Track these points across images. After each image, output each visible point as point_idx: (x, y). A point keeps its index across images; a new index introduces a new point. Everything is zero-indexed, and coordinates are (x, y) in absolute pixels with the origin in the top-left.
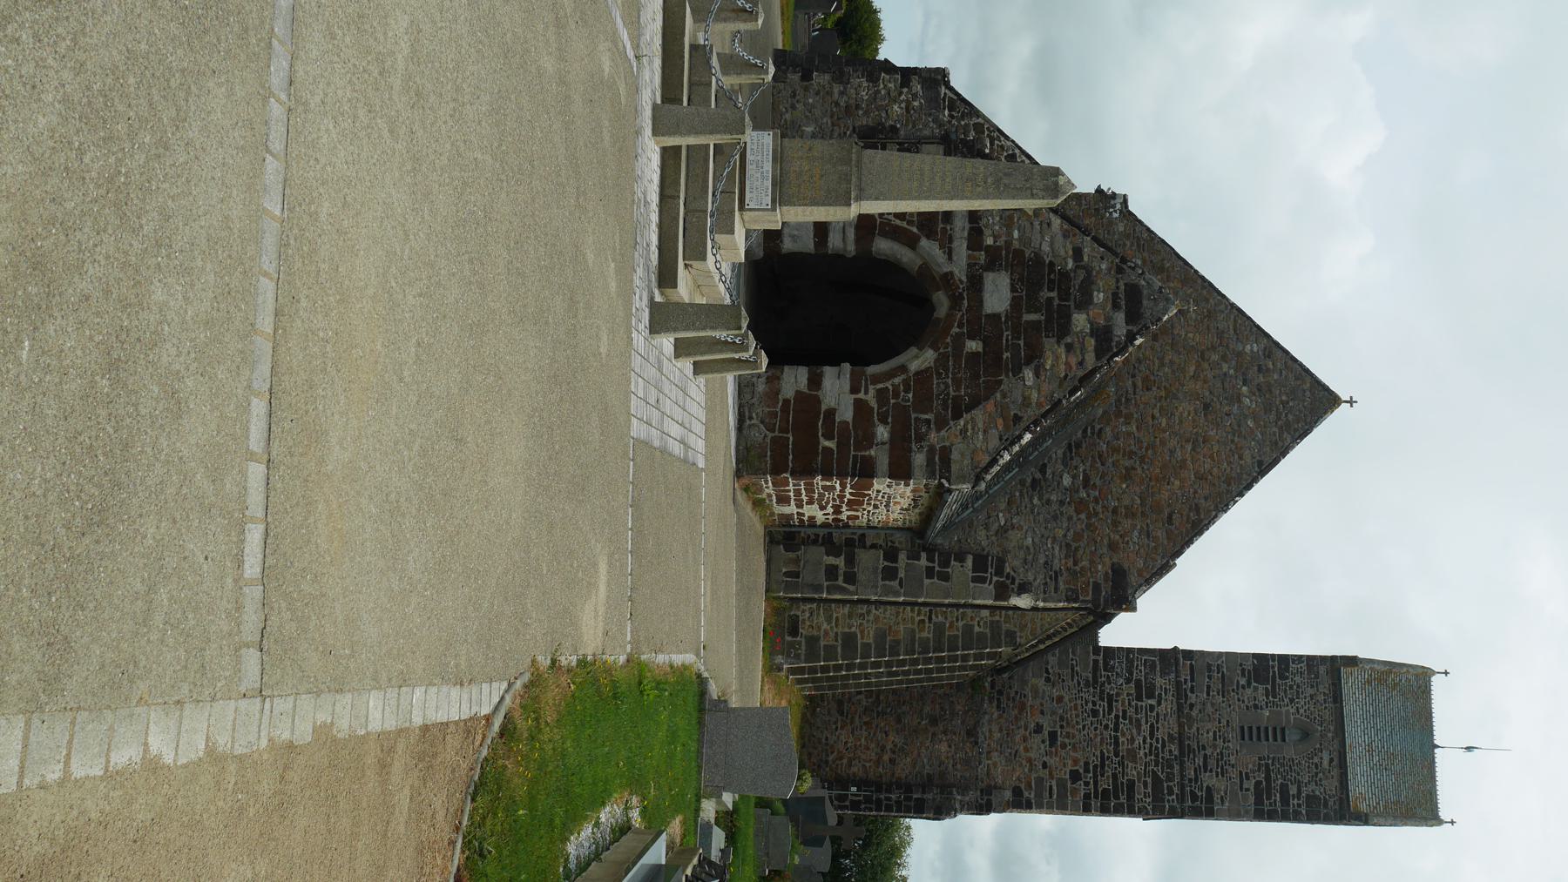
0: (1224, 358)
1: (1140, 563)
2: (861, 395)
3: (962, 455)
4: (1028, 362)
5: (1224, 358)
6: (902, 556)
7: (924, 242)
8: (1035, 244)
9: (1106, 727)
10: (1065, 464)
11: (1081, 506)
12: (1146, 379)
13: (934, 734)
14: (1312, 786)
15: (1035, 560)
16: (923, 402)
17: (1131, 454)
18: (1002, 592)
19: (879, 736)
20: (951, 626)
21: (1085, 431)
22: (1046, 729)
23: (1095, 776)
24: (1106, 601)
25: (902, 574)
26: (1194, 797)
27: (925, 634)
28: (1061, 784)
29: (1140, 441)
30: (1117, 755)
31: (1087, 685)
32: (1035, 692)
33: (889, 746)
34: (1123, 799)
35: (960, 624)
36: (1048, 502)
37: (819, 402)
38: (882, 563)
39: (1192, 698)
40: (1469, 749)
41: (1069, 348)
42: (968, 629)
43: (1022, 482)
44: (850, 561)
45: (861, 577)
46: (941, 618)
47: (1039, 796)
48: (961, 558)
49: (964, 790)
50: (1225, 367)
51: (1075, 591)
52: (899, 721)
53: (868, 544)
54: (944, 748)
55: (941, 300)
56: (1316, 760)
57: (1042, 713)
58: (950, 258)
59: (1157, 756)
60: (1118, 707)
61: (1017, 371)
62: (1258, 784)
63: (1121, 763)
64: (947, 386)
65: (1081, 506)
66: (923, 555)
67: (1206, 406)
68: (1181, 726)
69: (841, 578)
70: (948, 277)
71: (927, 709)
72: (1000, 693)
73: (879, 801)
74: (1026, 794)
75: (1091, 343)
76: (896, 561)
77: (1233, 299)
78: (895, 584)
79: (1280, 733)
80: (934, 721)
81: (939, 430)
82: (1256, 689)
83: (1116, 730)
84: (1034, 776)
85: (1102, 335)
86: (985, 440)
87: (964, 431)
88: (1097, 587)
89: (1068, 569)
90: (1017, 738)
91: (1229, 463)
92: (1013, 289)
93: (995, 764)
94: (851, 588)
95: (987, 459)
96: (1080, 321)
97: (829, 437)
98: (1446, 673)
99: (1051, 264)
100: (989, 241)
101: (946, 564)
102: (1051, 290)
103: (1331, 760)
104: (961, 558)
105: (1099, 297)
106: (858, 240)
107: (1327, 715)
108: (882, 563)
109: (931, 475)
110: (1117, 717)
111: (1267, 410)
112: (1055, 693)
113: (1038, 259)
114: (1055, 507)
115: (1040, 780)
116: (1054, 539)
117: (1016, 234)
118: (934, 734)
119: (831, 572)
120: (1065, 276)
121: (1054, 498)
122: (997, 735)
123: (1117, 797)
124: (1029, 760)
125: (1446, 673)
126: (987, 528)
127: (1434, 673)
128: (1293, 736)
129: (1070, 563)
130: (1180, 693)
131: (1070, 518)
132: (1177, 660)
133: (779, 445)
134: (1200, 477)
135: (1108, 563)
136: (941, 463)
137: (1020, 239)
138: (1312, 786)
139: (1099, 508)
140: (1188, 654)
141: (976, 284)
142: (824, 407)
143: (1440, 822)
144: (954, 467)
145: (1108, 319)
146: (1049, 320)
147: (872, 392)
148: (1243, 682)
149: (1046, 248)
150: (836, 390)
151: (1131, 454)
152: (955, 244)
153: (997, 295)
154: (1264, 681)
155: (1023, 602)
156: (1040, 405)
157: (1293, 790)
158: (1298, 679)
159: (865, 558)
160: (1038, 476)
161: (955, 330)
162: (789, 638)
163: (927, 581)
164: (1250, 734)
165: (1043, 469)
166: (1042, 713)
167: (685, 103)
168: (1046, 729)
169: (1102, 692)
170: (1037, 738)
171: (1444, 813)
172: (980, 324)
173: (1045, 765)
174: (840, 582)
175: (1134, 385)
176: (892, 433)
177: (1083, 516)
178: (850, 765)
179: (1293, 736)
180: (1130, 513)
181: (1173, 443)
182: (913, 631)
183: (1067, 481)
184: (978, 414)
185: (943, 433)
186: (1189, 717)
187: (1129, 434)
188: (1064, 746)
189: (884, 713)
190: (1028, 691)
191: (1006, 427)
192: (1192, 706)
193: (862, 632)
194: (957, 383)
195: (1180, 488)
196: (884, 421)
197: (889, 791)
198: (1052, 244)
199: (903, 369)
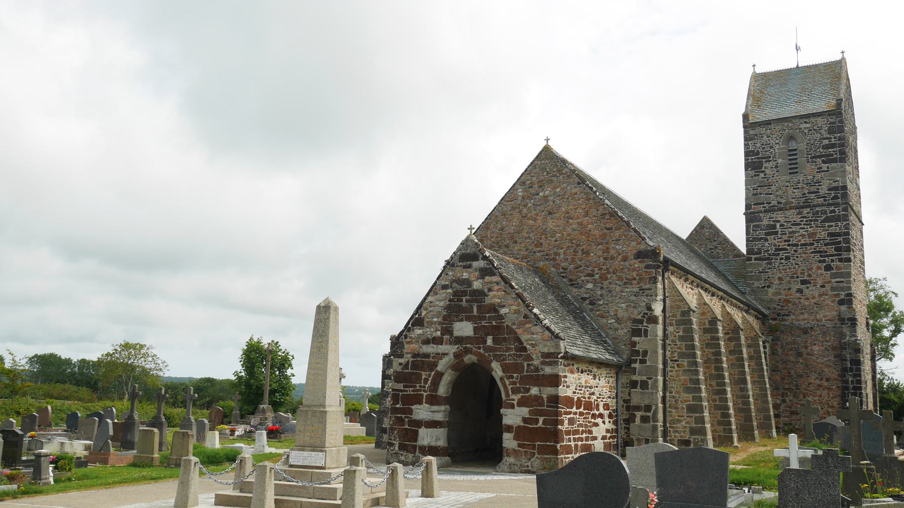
0: (525, 206)
1: (634, 244)
2: (515, 403)
3: (545, 346)
4: (497, 311)
5: (525, 206)
6: (634, 378)
7: (439, 368)
8: (440, 309)
9: (796, 251)
10: (581, 287)
11: (603, 278)
12: (536, 246)
13: (808, 354)
14: (823, 131)
15: (633, 302)
16: (517, 368)
17: (575, 252)
18: (653, 320)
19: (811, 388)
20: (679, 348)
21: (563, 277)
22: (800, 286)
23: (827, 256)
24: (655, 261)
25: (644, 378)
26: (836, 197)
27: (686, 364)
28: (834, 276)
29: (568, 247)
30: (813, 244)
31: (770, 264)
32: (777, 294)
33: (818, 382)
34: (840, 239)
35: (678, 343)
36: (601, 295)
37: (519, 426)
38: (638, 389)
39: (774, 203)
40: (797, 49)
41: (490, 290)
42: (681, 338)
43: (591, 310)
44: (638, 408)
45: (647, 402)
46: (676, 355)
47: (842, 289)
48: (634, 344)
49: (843, 335)
50: (530, 205)
51: (650, 279)
52: (801, 376)
53: (628, 398)
54: (816, 348)
55: (469, 359)
56: (806, 131)
57: (789, 289)
58: (447, 354)
59: (811, 221)
60: (782, 245)
61: (501, 317)
62: (824, 162)
63: (818, 241)
64: (510, 355)
65: (603, 278)
66: (633, 365)
67: (550, 213)
68: (791, 208)
69: (648, 414)
70: (456, 355)
71: (792, 359)
72: (779, 315)
73: (854, 388)
74: (842, 297)
75: (487, 279)
76: (637, 381)
77: (496, 203)
78: (650, 382)
79: (792, 152)
80: (799, 354)
81: (532, 359)
82: (766, 168)
83: (797, 245)
84: (830, 293)
85: (485, 273)
86: (537, 333)
87: (533, 345)
88: (647, 267)
89: (638, 283)
90: (807, 303)
91: (579, 199)
92: (462, 320)
93: (825, 316)
94: (653, 408)
95: (547, 332)
96: (477, 285)
97: (537, 421)
98: (754, 66)
99: (450, 301)
100: (439, 333)
101: (637, 353)
102: (462, 301)
103: (806, 122)
104: (634, 344)
105: (465, 275)
106: (439, 404)
107: (778, 128)
108: (638, 389)
109: (556, 363)
110: (789, 245)
111: (552, 182)
112: (777, 282)
113: (447, 308)
114: (604, 292)
115: (833, 289)
116: (622, 291)
117: (435, 320)
118: (808, 354)
119: (645, 419)
120: (455, 293)
121: (599, 293)
122: (806, 316)
123: (840, 243)
124: (820, 296)
125: (754, 66)
126: (616, 329)
127: (754, 72)
128: (793, 145)
129: (635, 282)
130: (771, 210)
131: (610, 283)
132: (752, 213)
133: (543, 450)
134: (587, 214)
135: (635, 261)
136: (550, 358)
137: (438, 317)
138: (823, 131)
139: (604, 267)
140: (748, 207)
141: (459, 340)
142: (522, 424)
143: (843, 59)
144: (552, 351)
145: (476, 270)
146: (476, 301)
147: (513, 397)
148: (762, 175)
149: (442, 304)
150: (513, 417)
151: (575, 252)
152: (440, 352)
153: (464, 329)
154: (761, 164)
155: (658, 309)
156: (519, 305)
157: (826, 142)
158: (758, 145)
159: (635, 400)
160: (587, 301)
161: (481, 351)
162: (692, 446)
163: (648, 363)
164: (793, 169)
165: (584, 299)
166: (789, 289)
167: (251, 495)
168: (800, 286)
169: (774, 254)
170: (806, 291)
171: (838, 57)
172: (478, 339)
173: (823, 286)
174: (650, 414)
175: (540, 251)
176: (535, 385)
177: (609, 276)
178: (833, 407)
179: (793, 145)
180: (607, 250)
181: (569, 230)
182: (684, 371)
183: (590, 286)
184: (524, 338)
185: (534, 357)
186: (786, 204)
187: (565, 253)
188: (809, 275)
189: (797, 385)
190: (777, 298)
191: (529, 322)
192: (779, 203)
193: (686, 401)
194: (508, 349)
195: (592, 224)
196: (528, 390)
197: (847, 382)
198: (440, 301)
199: (502, 379)
